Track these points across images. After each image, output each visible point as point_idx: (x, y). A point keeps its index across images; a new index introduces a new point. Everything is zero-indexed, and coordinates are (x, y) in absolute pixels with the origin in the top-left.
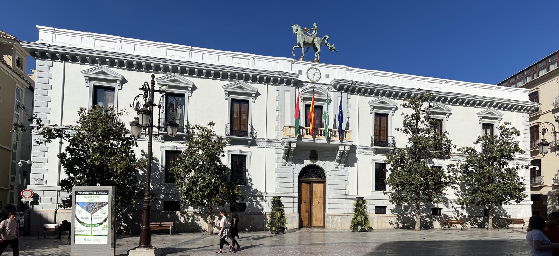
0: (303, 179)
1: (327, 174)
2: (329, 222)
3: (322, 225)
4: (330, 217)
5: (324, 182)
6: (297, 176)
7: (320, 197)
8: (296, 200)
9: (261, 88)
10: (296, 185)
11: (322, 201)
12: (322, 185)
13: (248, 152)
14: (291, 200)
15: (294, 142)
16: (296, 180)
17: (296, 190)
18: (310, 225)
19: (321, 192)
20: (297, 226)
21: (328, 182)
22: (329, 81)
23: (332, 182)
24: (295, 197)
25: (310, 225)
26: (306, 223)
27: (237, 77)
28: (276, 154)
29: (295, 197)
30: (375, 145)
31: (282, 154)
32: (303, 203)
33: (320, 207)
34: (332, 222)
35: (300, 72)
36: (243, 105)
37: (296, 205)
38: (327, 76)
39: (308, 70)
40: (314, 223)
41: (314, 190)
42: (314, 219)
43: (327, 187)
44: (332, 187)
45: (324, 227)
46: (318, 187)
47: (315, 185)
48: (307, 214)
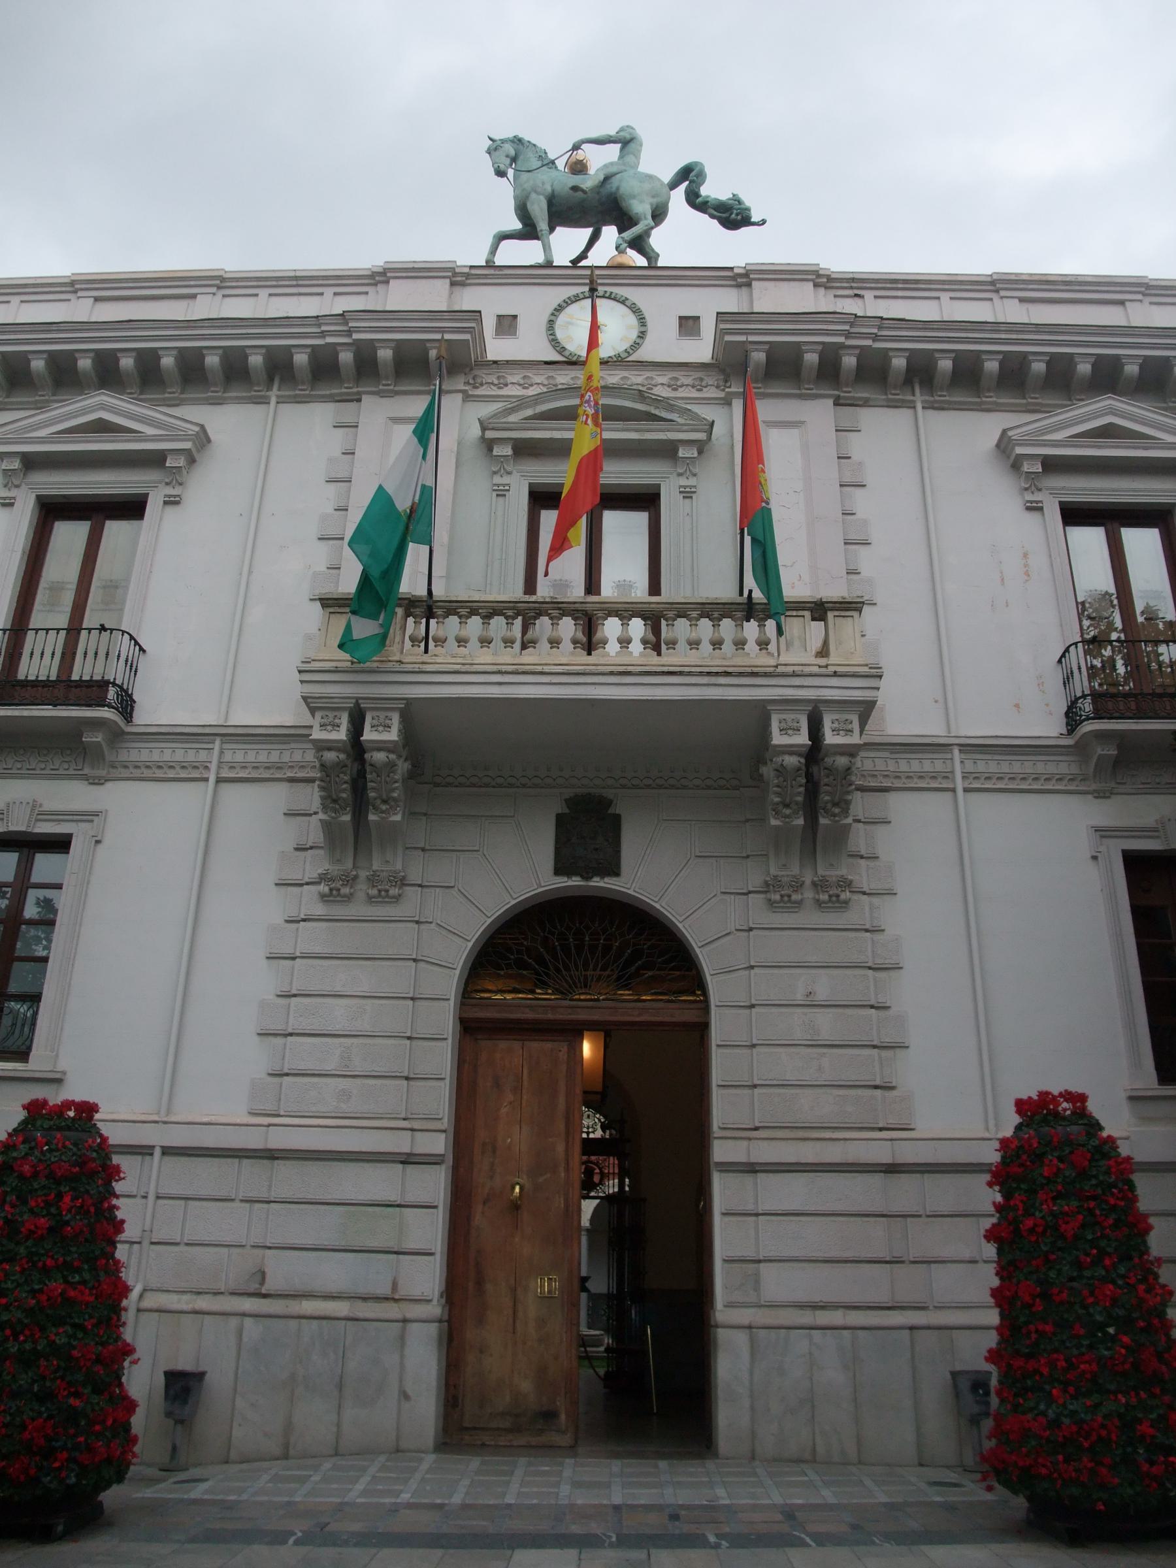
4: (741, 1339)
6: (449, 984)
8: (434, 1185)
9: (230, 424)
13: (88, 816)
14: (379, 1183)
15: (384, 704)
16: (444, 1018)
17: (438, 1100)
22: (701, 350)
27: (157, 1152)
28: (265, 829)
29: (407, 1160)
30: (1098, 715)
31: (313, 830)
35: (507, 324)
36: (115, 531)
37: (429, 1231)
38: (688, 325)
39: (559, 309)
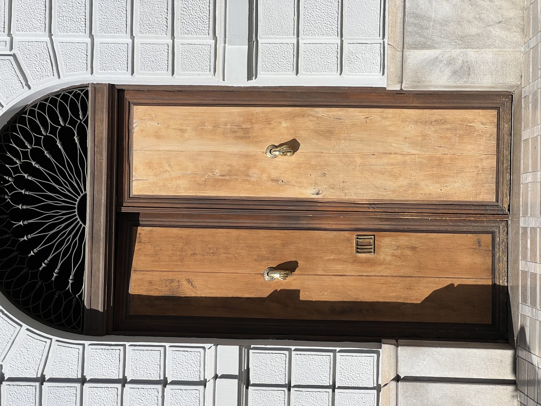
0: (94, 293)
1: (45, 83)
2: (467, 69)
3: (483, 121)
4: (415, 57)
5: (119, 99)
6: (65, 354)
7: (243, 134)
8: (268, 361)
10: (143, 357)
11: (282, 122)
12: (144, 121)
16: (102, 357)
18: (488, 219)
19: (200, 130)
20: (494, 361)
21: (112, 73)
23: (112, 39)
24: (244, 379)
25: (488, 219)
26: (461, 263)
32: (292, 282)
33: (328, 133)
34: (465, 41)
40: (468, 183)
41: (184, 189)
42: (431, 190)
43: (145, 77)
44: (153, 41)
45: (501, 103)
46: (164, 160)
47: (144, 181)
48: (388, 245)
